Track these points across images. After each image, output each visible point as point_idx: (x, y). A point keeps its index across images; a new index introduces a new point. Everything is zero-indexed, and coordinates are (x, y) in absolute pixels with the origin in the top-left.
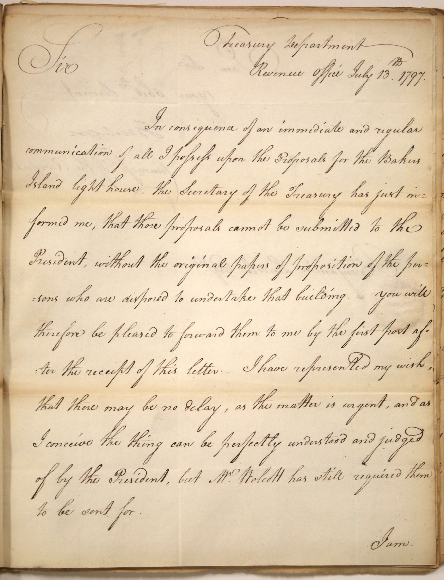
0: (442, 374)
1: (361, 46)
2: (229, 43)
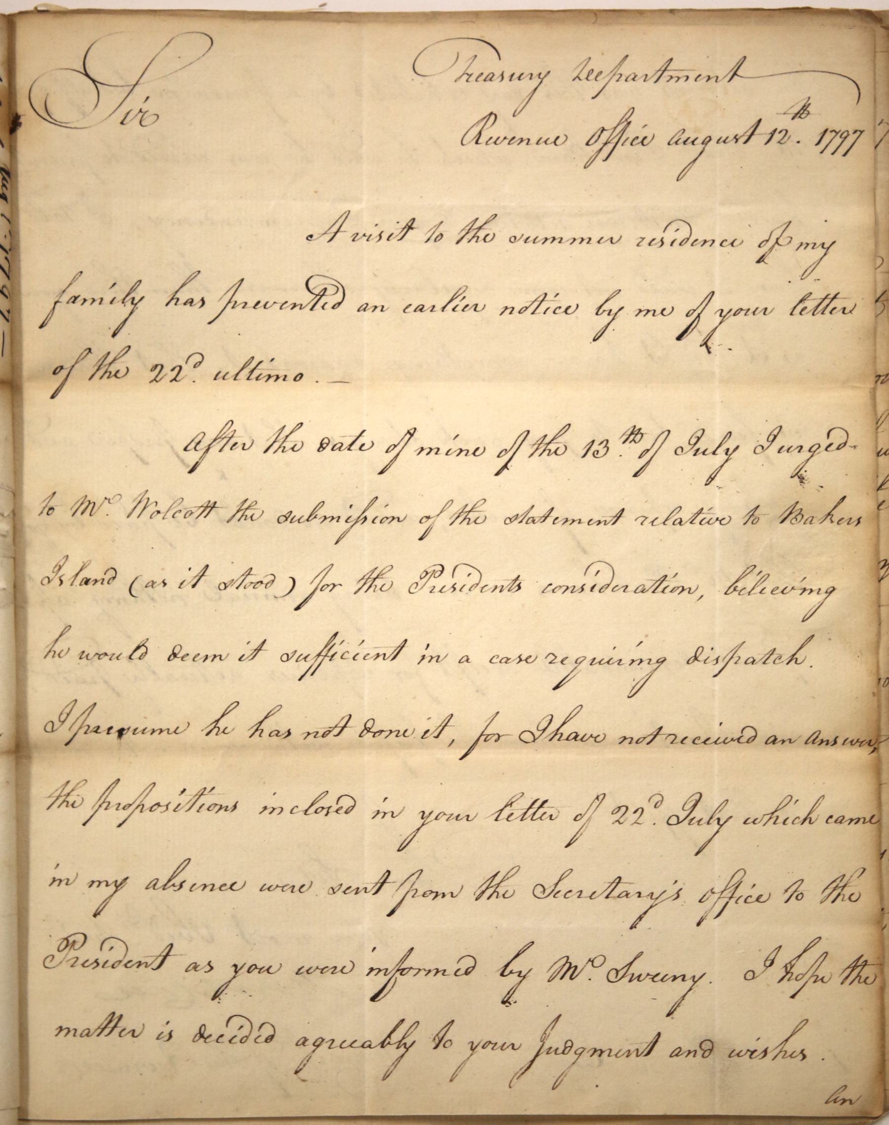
0: (883, 733)
1: (736, 77)
2: (579, 76)
